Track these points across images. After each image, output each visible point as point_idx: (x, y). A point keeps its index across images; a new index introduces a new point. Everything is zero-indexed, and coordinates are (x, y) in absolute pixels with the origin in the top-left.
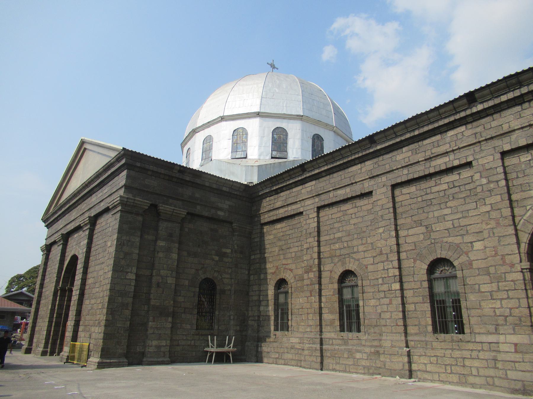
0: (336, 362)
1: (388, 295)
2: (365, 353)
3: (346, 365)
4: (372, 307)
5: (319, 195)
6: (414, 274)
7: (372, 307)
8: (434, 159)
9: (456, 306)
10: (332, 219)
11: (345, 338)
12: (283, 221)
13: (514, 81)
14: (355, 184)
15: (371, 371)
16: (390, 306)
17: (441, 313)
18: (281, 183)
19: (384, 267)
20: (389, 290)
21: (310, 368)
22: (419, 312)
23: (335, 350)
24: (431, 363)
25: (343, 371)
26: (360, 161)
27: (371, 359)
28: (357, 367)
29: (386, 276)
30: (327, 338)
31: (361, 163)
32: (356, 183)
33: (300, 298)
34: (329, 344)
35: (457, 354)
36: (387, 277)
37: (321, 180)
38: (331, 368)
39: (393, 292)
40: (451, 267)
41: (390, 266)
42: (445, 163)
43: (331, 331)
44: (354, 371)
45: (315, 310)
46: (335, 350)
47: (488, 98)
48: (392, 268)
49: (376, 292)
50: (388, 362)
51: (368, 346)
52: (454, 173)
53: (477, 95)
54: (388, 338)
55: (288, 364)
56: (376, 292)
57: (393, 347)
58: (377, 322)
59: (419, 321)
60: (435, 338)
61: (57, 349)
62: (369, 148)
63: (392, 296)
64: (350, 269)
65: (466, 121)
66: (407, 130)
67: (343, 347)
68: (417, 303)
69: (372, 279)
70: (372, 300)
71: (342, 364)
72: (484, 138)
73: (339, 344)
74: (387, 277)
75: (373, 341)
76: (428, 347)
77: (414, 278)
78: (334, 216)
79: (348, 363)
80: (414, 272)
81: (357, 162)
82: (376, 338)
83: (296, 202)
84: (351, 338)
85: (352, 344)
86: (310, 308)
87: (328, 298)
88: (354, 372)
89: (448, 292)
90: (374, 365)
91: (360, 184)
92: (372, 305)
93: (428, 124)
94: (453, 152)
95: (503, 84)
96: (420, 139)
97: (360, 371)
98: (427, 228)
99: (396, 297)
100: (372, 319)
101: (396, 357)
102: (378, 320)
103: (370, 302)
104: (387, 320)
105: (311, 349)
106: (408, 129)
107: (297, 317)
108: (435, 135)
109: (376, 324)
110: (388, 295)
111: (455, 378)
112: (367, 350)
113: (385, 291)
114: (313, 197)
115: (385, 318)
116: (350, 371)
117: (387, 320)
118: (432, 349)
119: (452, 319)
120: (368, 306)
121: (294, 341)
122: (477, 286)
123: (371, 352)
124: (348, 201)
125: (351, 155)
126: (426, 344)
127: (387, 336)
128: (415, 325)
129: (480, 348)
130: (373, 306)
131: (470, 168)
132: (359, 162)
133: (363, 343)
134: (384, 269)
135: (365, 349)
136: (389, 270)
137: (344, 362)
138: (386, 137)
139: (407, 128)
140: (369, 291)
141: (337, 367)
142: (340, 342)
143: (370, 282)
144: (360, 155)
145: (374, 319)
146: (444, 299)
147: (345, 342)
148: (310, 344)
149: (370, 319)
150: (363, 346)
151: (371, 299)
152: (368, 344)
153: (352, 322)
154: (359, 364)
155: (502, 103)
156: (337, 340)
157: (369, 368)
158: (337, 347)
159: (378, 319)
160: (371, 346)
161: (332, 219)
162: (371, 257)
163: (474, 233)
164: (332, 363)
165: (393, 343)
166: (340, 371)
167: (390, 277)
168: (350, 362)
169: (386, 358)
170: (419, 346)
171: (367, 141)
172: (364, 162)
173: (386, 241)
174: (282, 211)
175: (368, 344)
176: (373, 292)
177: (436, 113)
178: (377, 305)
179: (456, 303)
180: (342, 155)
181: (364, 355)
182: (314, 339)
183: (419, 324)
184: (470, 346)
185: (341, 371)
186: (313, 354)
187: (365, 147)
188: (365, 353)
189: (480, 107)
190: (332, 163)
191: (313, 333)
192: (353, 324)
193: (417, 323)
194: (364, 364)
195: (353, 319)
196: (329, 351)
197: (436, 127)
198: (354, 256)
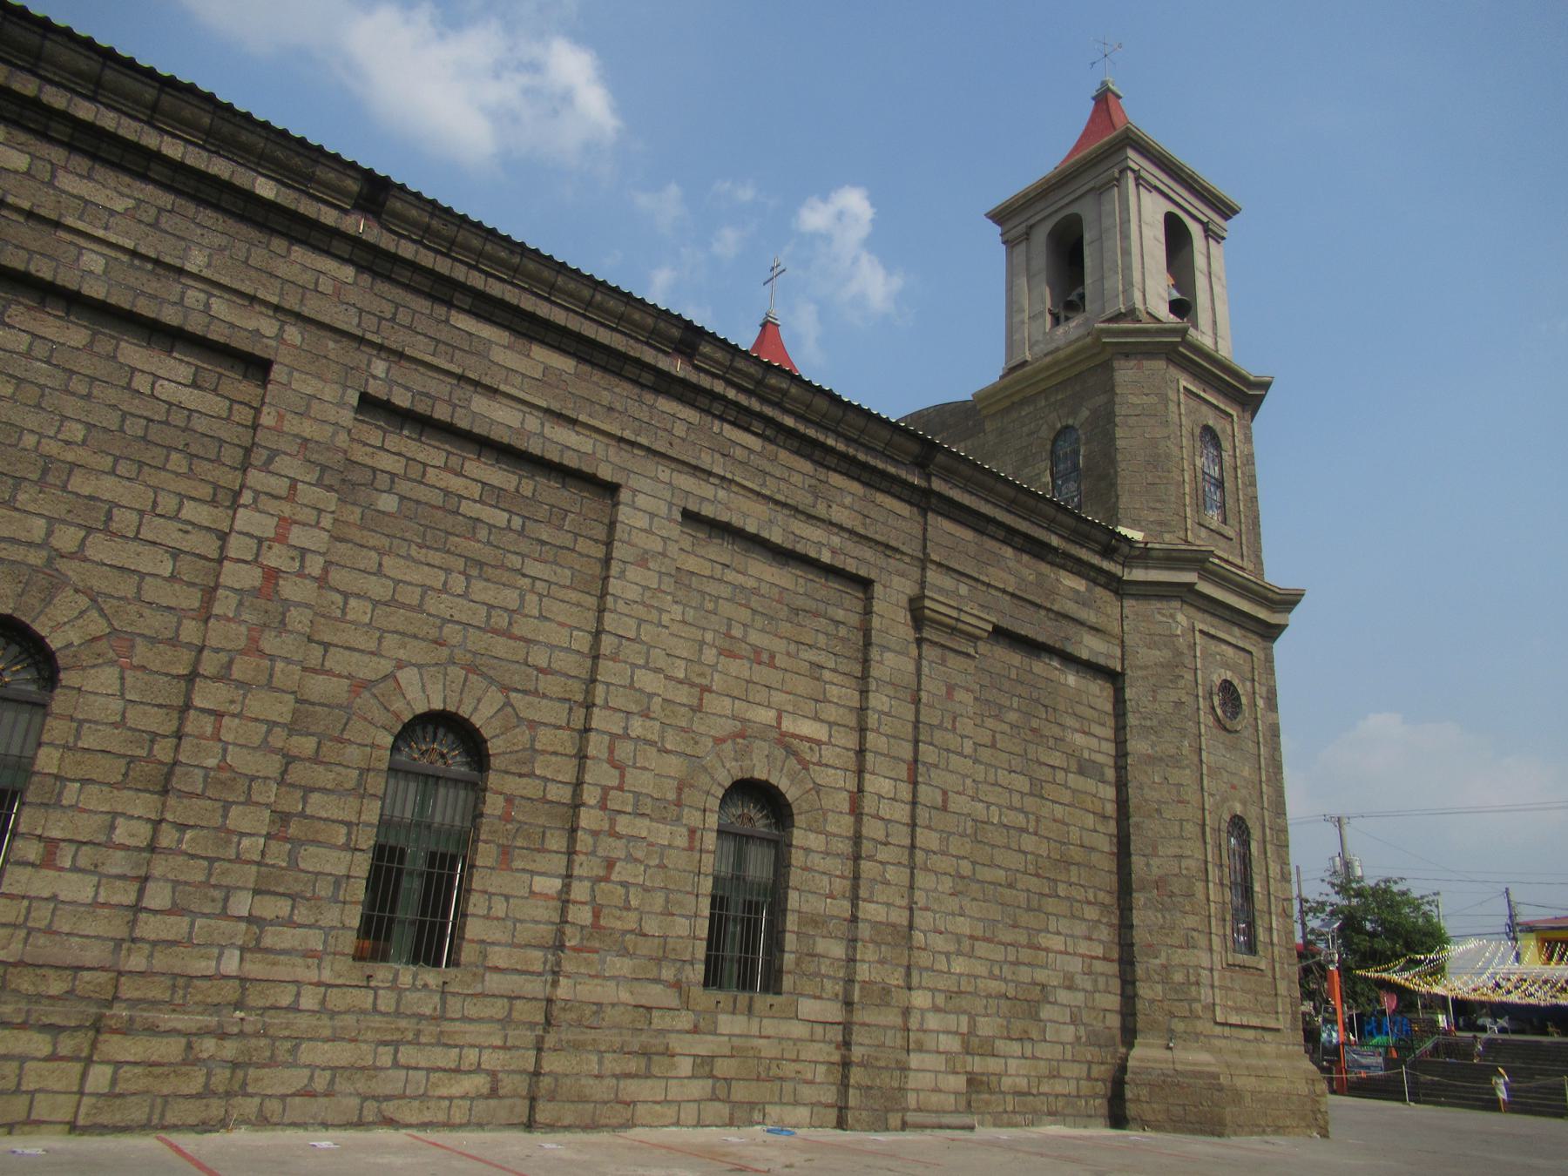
8: (803, 518)
9: (387, 868)
17: (385, 892)
37: (383, 287)
52: (175, 354)
53: (169, 98)
61: (379, 1160)
65: (452, 297)
83: (710, 474)
89: (738, 878)
94: (360, 343)
95: (84, 63)
106: (100, 91)
108: (692, 405)
124: (553, 474)
131: (479, 456)
146: (402, 844)
153: (391, 921)
155: (157, 156)
179: (442, 867)
197: (165, 156)
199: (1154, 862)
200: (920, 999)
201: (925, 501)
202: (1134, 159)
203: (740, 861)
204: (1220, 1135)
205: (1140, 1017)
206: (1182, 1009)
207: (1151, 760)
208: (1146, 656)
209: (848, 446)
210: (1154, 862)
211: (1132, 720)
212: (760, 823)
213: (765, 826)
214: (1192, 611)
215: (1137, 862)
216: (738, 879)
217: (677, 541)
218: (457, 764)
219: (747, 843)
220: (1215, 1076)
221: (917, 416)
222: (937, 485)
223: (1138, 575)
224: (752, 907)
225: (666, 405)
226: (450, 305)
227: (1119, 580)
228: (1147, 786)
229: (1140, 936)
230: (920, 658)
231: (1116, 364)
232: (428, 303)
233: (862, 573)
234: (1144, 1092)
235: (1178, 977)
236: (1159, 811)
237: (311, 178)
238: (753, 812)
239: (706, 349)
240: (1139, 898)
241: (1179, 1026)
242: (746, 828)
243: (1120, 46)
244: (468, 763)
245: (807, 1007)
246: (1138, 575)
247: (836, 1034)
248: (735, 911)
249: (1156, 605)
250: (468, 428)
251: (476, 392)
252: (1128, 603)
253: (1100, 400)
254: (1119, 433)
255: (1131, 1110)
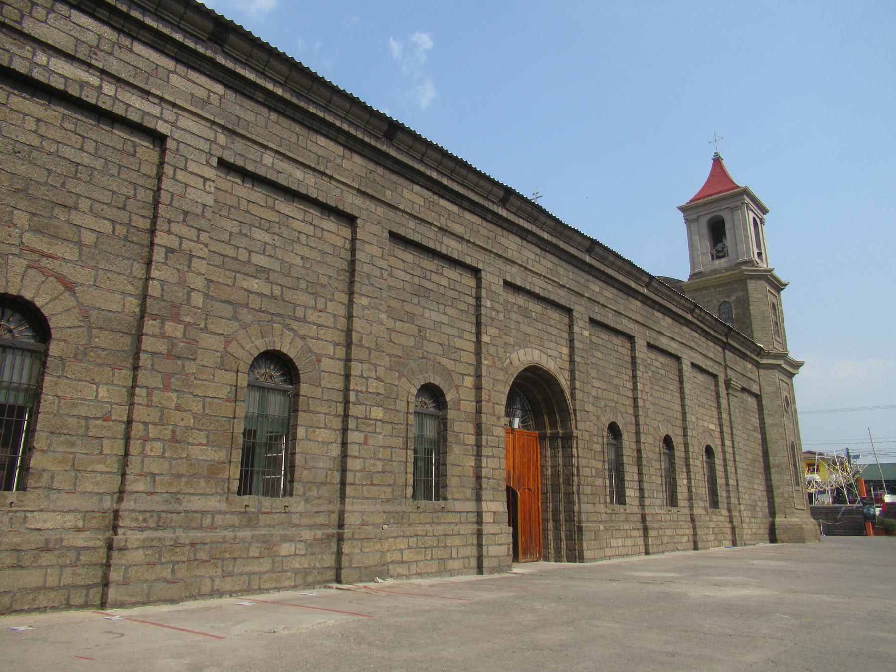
0: (223, 571)
1: (362, 427)
2: (301, 541)
3: (253, 574)
4: (320, 445)
5: (233, 133)
6: (397, 398)
7: (320, 445)
10: (247, 211)
11: (252, 510)
12: (33, 96)
13: (612, 258)
14: (327, 179)
15: (310, 579)
16: (365, 447)
18: (426, 164)
19: (362, 371)
20: (366, 418)
21: (144, 604)
22: (395, 463)
23: (225, 541)
24: (409, 547)
25: (240, 591)
26: (348, 145)
27: (312, 554)
28: (279, 574)
29: (364, 389)
30: (195, 512)
31: (345, 147)
32: (331, 177)
33: (97, 385)
34: (200, 528)
35: (439, 529)
36: (365, 392)
38: (206, 589)
39: (372, 422)
40: (21, 325)
41: (373, 374)
42: (145, 113)
43: (208, 491)
44: (270, 587)
45: (174, 432)
46: (225, 541)
47: (150, 6)
48: (375, 379)
49: (332, 415)
50: (358, 553)
51: (306, 526)
54: (356, 507)
55: (16, 607)
56: (332, 415)
57: (364, 525)
58: (326, 477)
59: (395, 480)
60: (415, 507)
62: (377, 138)
63: (370, 429)
64: (285, 352)
66: (179, 23)
67: (247, 533)
68: (395, 448)
69: (328, 387)
70: (322, 430)
71: (241, 574)
72: (439, 225)
73: (230, 526)
74: (365, 392)
75: (315, 515)
76: (404, 521)
77: (395, 405)
78: (254, 209)
79: (256, 569)
80: (397, 394)
81: (342, 139)
82: (322, 508)
84: (267, 510)
85: (268, 523)
86: (155, 424)
87: (210, 404)
88: (271, 589)
90: (317, 565)
91: (337, 187)
92: (320, 439)
93: (459, 183)
95: (588, 244)
96: (224, 81)
97: (287, 583)
98: (420, 331)
99: (375, 432)
100: (317, 468)
101: (372, 543)
102: (329, 472)
103: (317, 433)
104: (357, 474)
105: (154, 543)
107: (73, 444)
109: (324, 480)
110: (362, 427)
111: (433, 566)
112: (307, 534)
113: (358, 418)
114: (213, 123)
115: (354, 469)
116: (260, 589)
117: (357, 474)
118: (409, 525)
119: (421, 477)
120: (313, 440)
121: (49, 525)
122: (462, 435)
123: (315, 539)
125: (343, 119)
126: (402, 517)
127: (353, 504)
128: (389, 485)
129: (458, 520)
130: (323, 442)
132: (344, 143)
133: (295, 519)
134: (362, 376)
135: (303, 533)
136: (371, 380)
137: (247, 569)
138: (410, 148)
139: (440, 163)
140: (318, 409)
141: (228, 585)
142: (236, 519)
143: (323, 393)
144: (360, 135)
145: (321, 468)
147: (250, 519)
148: (141, 529)
149: (313, 467)
150: (293, 527)
151: (319, 428)
152: (306, 521)
153: (252, 472)
154: (285, 569)
156: (228, 516)
157: (306, 572)
158: (229, 534)
159: (330, 470)
160: (311, 527)
161: (247, 211)
162: (330, 342)
163: (466, 363)
164: (210, 577)
165: (365, 518)
166: (231, 594)
167: (371, 393)
168: (265, 565)
169: (354, 547)
170: (392, 521)
171: (385, 127)
172: (352, 150)
173: (371, 325)
174: (60, 66)
175: (306, 521)
176: (326, 414)
177: (438, 157)
178: (330, 440)
180: (329, 101)
181: (301, 546)
182: (163, 515)
183: (394, 484)
184: (450, 518)
185: (235, 592)
186: (163, 560)
187: (373, 130)
188: (301, 541)
189: (504, 213)
190: (298, 95)
191: (156, 498)
192: (255, 477)
193: (391, 482)
194: (297, 566)
195: (256, 464)
196: (207, 547)
198: (295, 325)
199: (776, 459)
200: (742, 507)
201: (725, 346)
202: (747, 200)
203: (263, 403)
204: (804, 542)
205: (776, 508)
206: (788, 505)
207: (772, 425)
208: (767, 389)
209: (196, 44)
210: (776, 459)
211: (765, 411)
212: (277, 378)
213: (433, 407)
214: (779, 373)
215: (771, 459)
216: (262, 416)
217: (213, 181)
218: (24, 335)
219: (268, 392)
220: (801, 525)
221: (658, 277)
222: (730, 342)
223: (764, 361)
224: (428, 452)
225: (685, 328)
226: (653, 308)
227: (758, 363)
228: (772, 435)
229: (774, 483)
230: (728, 399)
231: (748, 281)
232: (342, 149)
233: (475, 265)
234: (781, 531)
235: (786, 495)
236: (776, 442)
237: (640, 279)
238: (276, 374)
239: (232, 38)
240: (773, 471)
241: (788, 510)
242: (269, 383)
243: (722, 138)
244: (34, 337)
245: (459, 506)
246: (764, 361)
247: (473, 518)
248: (421, 455)
249: (770, 371)
250: (139, 122)
251: (444, 235)
252: (761, 371)
253: (741, 293)
254: (751, 308)
255: (778, 537)
